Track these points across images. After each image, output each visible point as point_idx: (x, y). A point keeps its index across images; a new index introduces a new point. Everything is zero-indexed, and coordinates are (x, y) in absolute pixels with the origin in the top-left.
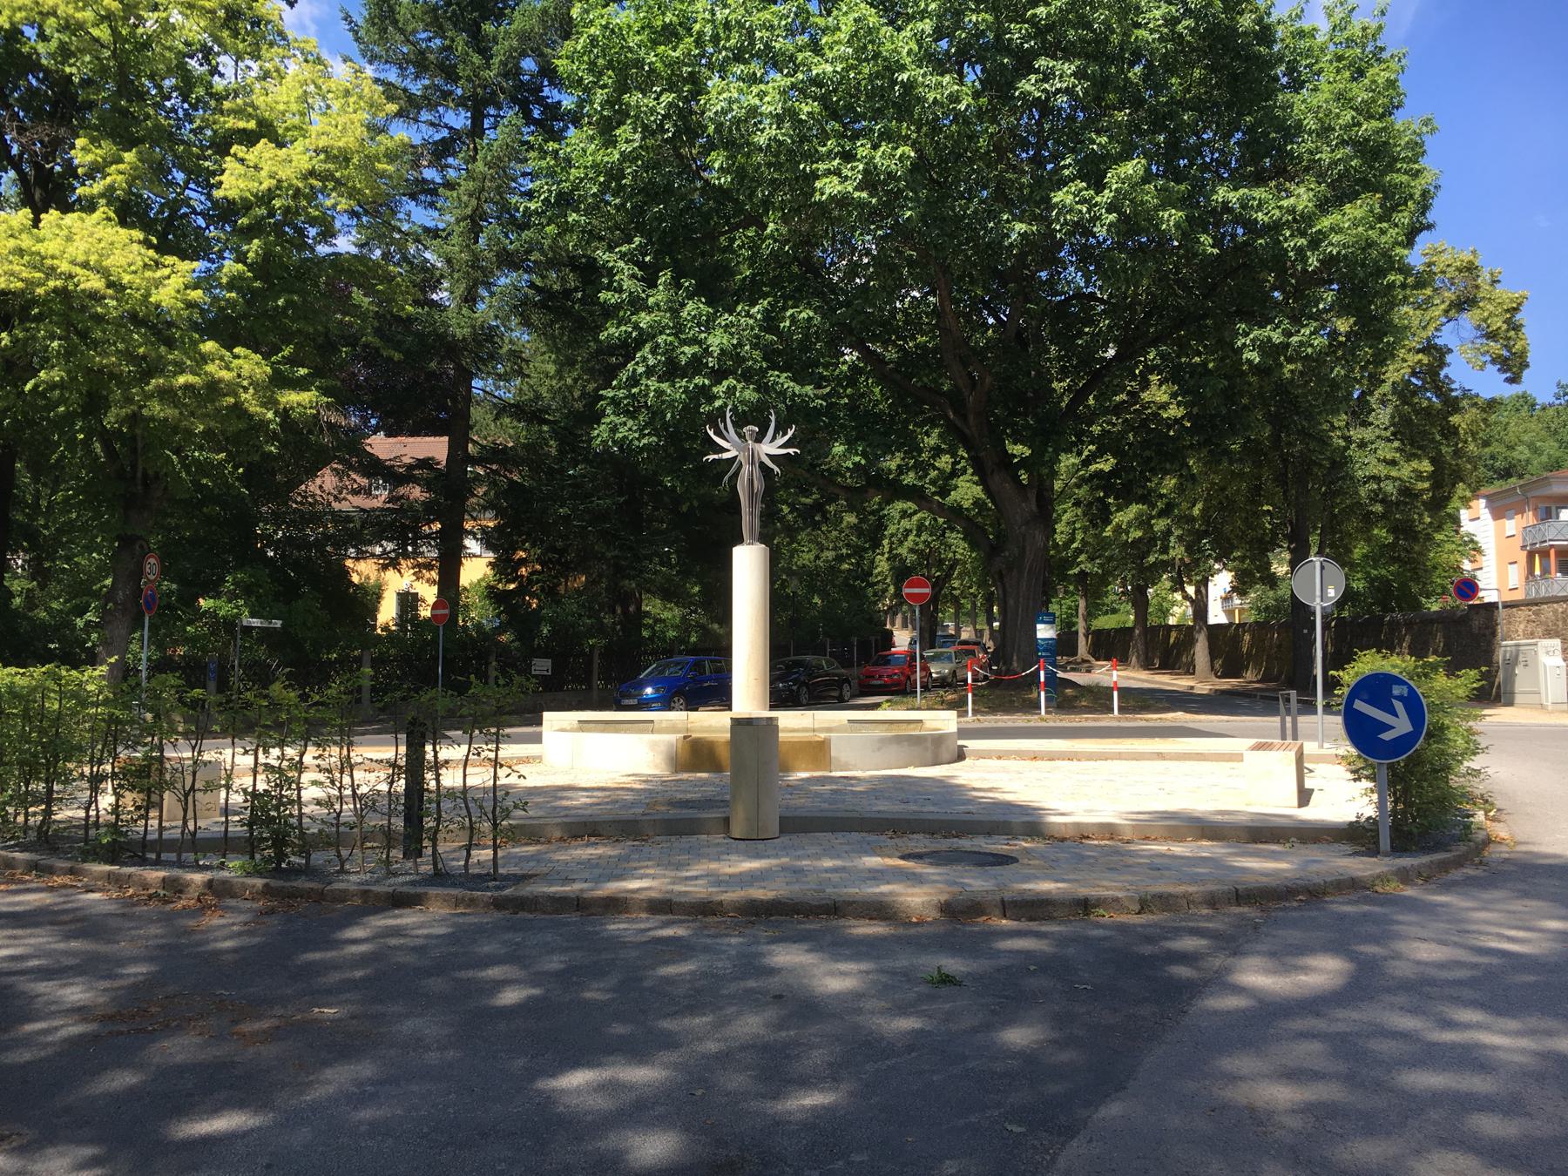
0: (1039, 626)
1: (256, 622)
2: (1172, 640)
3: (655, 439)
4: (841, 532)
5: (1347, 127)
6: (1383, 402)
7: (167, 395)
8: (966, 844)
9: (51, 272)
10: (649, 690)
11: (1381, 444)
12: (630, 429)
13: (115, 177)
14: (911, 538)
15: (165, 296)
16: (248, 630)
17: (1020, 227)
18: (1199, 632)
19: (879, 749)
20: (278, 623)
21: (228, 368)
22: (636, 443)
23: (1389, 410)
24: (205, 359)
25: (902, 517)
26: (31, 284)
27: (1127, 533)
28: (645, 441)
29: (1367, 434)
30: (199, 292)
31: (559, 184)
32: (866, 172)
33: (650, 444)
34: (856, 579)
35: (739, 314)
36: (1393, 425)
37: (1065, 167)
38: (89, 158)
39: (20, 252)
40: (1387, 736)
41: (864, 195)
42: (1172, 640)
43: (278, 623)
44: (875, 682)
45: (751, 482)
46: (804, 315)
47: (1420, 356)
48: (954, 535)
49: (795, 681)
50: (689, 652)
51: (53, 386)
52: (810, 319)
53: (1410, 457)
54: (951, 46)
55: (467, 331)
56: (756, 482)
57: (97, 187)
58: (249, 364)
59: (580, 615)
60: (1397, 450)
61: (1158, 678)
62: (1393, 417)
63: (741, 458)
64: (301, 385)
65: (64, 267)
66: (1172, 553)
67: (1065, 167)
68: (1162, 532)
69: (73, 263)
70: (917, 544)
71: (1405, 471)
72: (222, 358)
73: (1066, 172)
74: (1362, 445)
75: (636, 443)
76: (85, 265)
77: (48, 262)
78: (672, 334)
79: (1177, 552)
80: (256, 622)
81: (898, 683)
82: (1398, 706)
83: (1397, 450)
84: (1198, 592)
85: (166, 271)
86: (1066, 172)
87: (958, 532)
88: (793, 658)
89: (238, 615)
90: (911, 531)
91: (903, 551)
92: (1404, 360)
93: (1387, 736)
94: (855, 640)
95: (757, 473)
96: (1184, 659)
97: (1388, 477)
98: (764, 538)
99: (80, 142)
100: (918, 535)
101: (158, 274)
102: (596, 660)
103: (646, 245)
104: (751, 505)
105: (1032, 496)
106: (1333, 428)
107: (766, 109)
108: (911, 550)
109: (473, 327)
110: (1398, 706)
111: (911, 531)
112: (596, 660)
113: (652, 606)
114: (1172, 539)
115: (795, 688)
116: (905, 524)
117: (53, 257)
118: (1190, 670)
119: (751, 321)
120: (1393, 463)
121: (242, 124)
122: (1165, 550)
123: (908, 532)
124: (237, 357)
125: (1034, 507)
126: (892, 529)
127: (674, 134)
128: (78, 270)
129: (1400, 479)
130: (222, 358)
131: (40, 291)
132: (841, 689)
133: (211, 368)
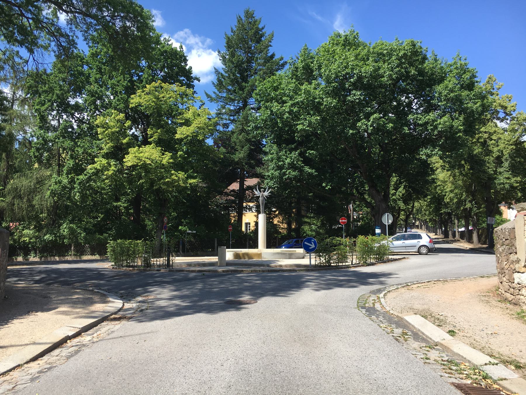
0: (376, 230)
1: (190, 232)
5: (446, 96)
6: (506, 160)
7: (164, 183)
8: (316, 278)
9: (141, 160)
11: (505, 173)
13: (156, 136)
15: (164, 162)
16: (189, 234)
17: (351, 131)
20: (195, 232)
21: (177, 177)
23: (508, 162)
24: (172, 174)
26: (138, 163)
29: (501, 170)
30: (172, 160)
36: (509, 167)
37: (361, 116)
38: (151, 133)
39: (136, 157)
40: (310, 248)
41: (308, 128)
43: (195, 232)
47: (512, 147)
48: (400, 202)
51: (143, 183)
53: (514, 176)
54: (224, 154)
57: (152, 139)
58: (181, 175)
60: (511, 174)
62: (509, 164)
64: (194, 178)
65: (144, 159)
66: (467, 206)
69: (145, 158)
71: (513, 180)
72: (175, 175)
73: (362, 117)
74: (500, 173)
76: (147, 158)
77: (141, 158)
80: (190, 232)
82: (313, 243)
83: (511, 174)
85: (166, 156)
86: (362, 117)
89: (186, 230)
92: (508, 148)
93: (310, 248)
97: (506, 183)
98: (265, 212)
99: (149, 130)
101: (164, 156)
106: (489, 168)
107: (286, 110)
110: (313, 243)
117: (142, 157)
120: (508, 178)
121: (181, 121)
124: (179, 174)
128: (146, 159)
130: (175, 175)
131: (139, 164)
133: (173, 177)
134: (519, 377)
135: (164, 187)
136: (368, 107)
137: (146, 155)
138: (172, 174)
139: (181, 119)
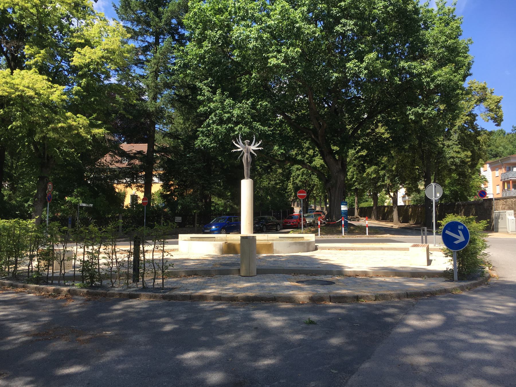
0: (342, 206)
1: (84, 205)
2: (386, 211)
3: (215, 144)
4: (277, 175)
6: (455, 132)
7: (55, 130)
8: (318, 278)
9: (17, 89)
10: (214, 227)
11: (454, 146)
12: (207, 141)
13: (38, 58)
14: (300, 177)
15: (54, 97)
16: (82, 207)
17: (336, 75)
18: (395, 208)
19: (289, 247)
20: (91, 205)
21: (75, 121)
22: (209, 146)
23: (457, 135)
24: (67, 118)
25: (297, 170)
26: (10, 93)
27: (371, 175)
28: (212, 145)
29: (450, 143)
30: (66, 96)
31: (184, 61)
32: (285, 57)
33: (214, 146)
34: (282, 190)
35: (243, 103)
36: (458, 140)
37: (350, 55)
38: (29, 52)
39: (7, 83)
40: (456, 242)
41: (284, 64)
42: (386, 211)
43: (91, 205)
44: (288, 225)
45: (247, 158)
46: (264, 104)
47: (467, 117)
48: (314, 176)
49: (262, 224)
50: (227, 215)
51: (17, 127)
52: (267, 105)
53: (464, 150)
55: (154, 109)
56: (249, 159)
57: (32, 62)
58: (82, 120)
59: (191, 203)
61: (381, 223)
62: (458, 137)
63: (244, 151)
64: (99, 127)
65: (21, 88)
66: (386, 182)
67: (350, 55)
68: (382, 175)
69: (24, 86)
70: (302, 179)
71: (463, 155)
72: (73, 118)
73: (351, 57)
74: (448, 146)
75: (209, 146)
76: (28, 87)
77: (16, 86)
78: (221, 110)
79: (387, 182)
80: (84, 205)
81: (296, 225)
82: (460, 232)
83: (460, 148)
84: (394, 195)
85: (55, 89)
86: (351, 57)
87: (315, 175)
88: (261, 216)
89: (78, 203)
90: (300, 175)
91: (297, 181)
92: (462, 119)
93: (456, 242)
94: (281, 211)
95: (249, 156)
96: (390, 217)
97: (457, 157)
98: (251, 177)
100: (302, 176)
101: (52, 90)
102: (196, 217)
103: (213, 81)
104: (247, 166)
105: (340, 163)
107: (252, 36)
108: (300, 181)
109: (156, 108)
110: (460, 232)
111: (300, 175)
112: (196, 217)
113: (215, 199)
114: (386, 177)
115: (262, 226)
116: (298, 172)
117: (17, 85)
118: (392, 220)
119: (247, 106)
121: (80, 41)
122: (383, 181)
123: (299, 175)
124: (78, 117)
125: (340, 167)
126: (293, 174)
127: (222, 44)
128: (26, 89)
129: (461, 158)
130: (73, 118)
131: (13, 96)
132: (277, 227)
133: (69, 121)
134: (347, 343)
135: (51, 134)
136: (361, 44)
137: (26, 82)
138: (67, 118)
139: (78, 37)
